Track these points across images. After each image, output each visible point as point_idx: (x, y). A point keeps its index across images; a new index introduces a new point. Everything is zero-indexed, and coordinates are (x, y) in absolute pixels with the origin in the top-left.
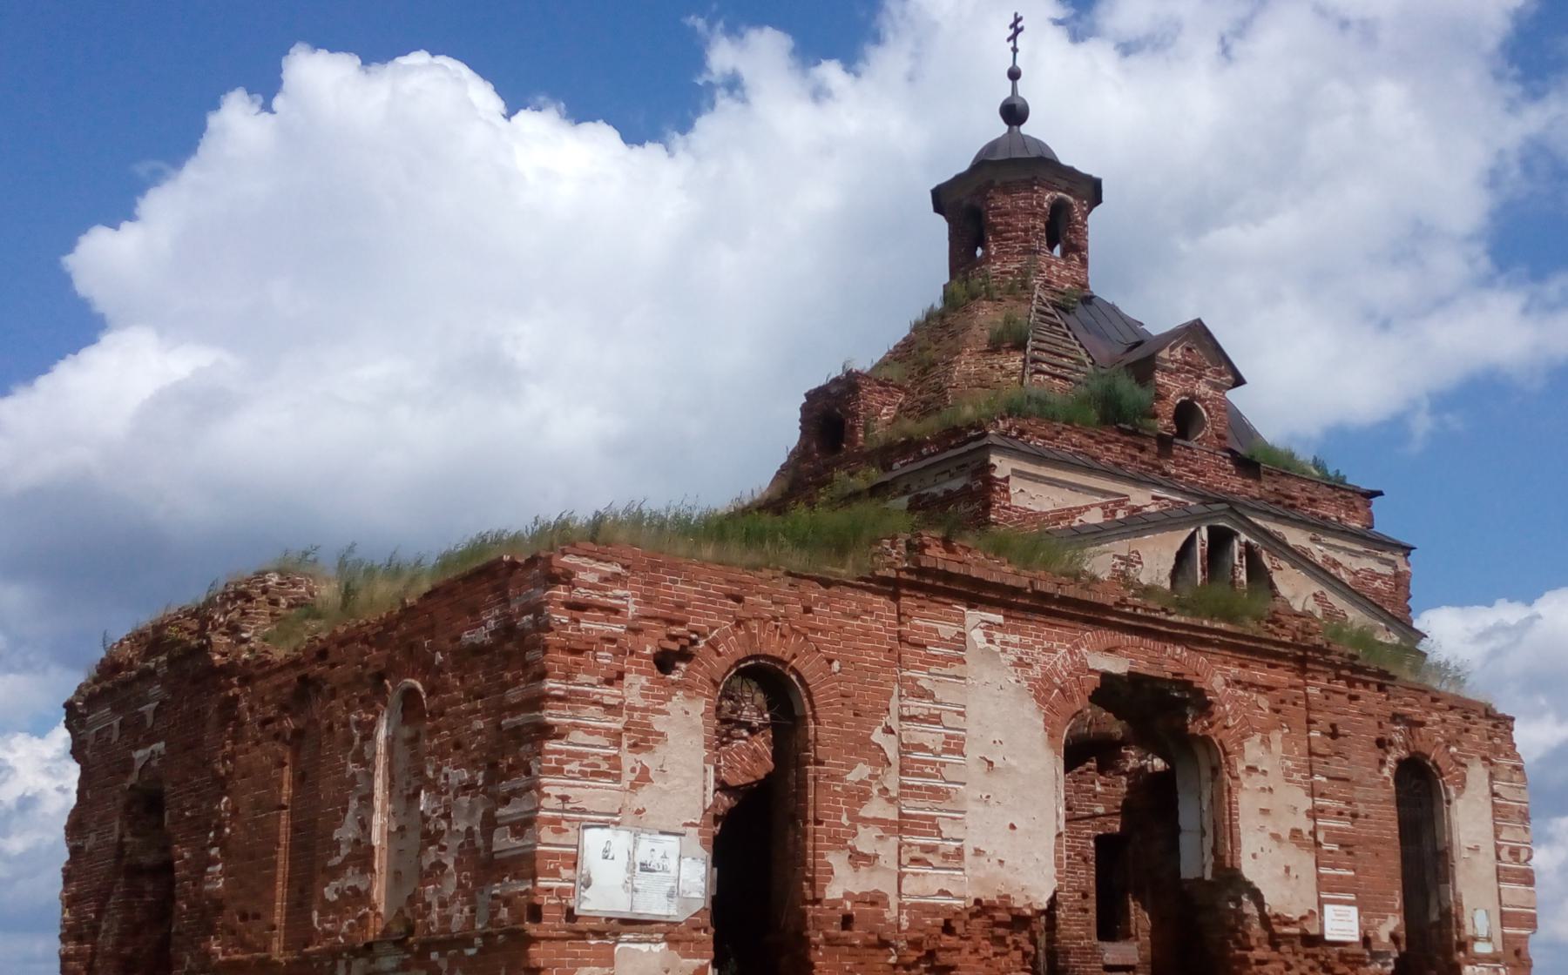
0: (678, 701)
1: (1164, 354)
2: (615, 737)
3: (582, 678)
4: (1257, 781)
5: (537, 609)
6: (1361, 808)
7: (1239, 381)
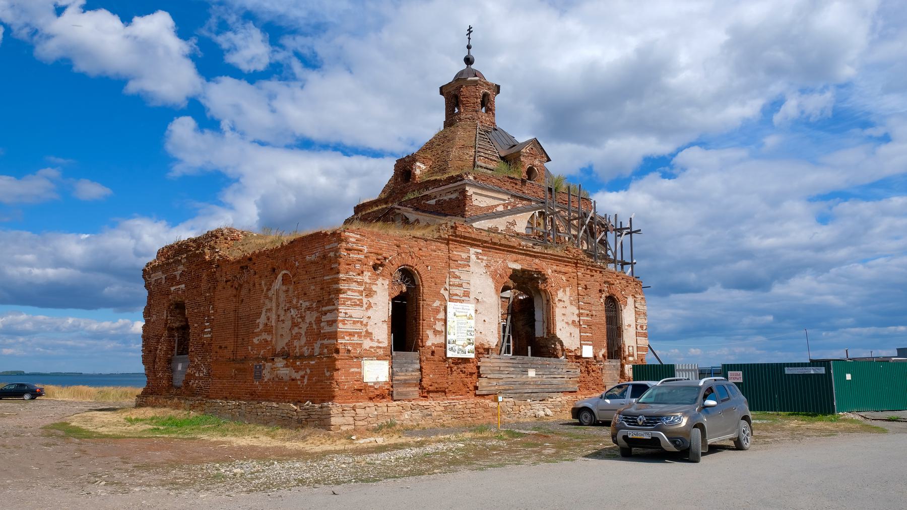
0: (380, 281)
1: (524, 150)
2: (361, 293)
3: (351, 273)
4: (560, 305)
5: (337, 250)
6: (594, 313)
7: (549, 160)
